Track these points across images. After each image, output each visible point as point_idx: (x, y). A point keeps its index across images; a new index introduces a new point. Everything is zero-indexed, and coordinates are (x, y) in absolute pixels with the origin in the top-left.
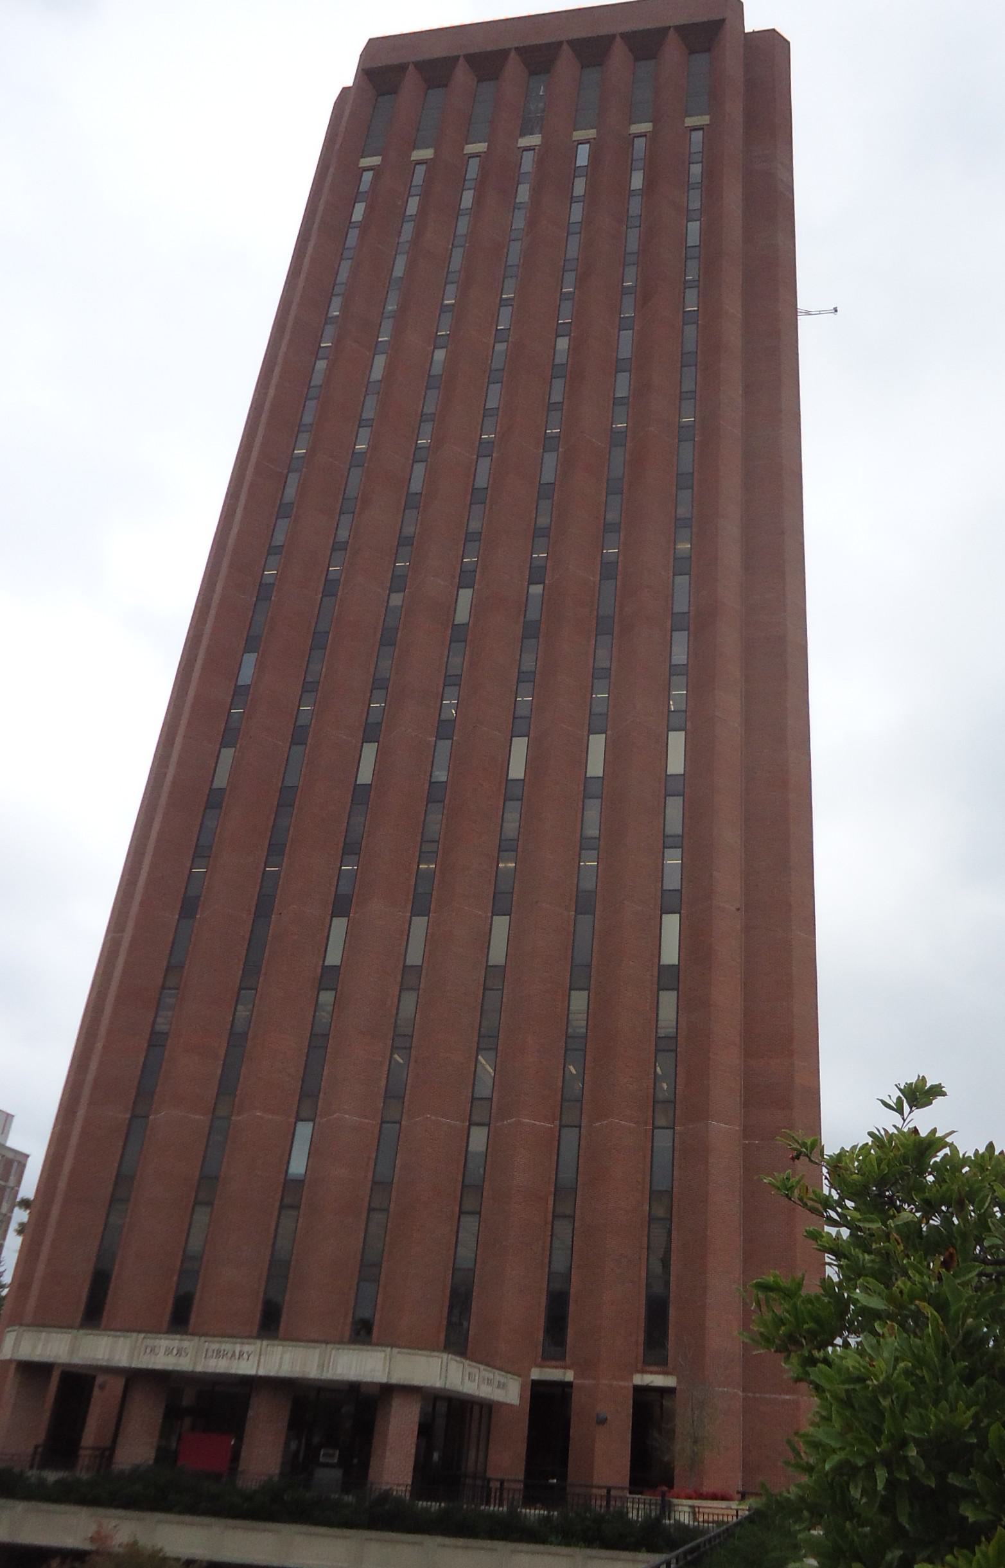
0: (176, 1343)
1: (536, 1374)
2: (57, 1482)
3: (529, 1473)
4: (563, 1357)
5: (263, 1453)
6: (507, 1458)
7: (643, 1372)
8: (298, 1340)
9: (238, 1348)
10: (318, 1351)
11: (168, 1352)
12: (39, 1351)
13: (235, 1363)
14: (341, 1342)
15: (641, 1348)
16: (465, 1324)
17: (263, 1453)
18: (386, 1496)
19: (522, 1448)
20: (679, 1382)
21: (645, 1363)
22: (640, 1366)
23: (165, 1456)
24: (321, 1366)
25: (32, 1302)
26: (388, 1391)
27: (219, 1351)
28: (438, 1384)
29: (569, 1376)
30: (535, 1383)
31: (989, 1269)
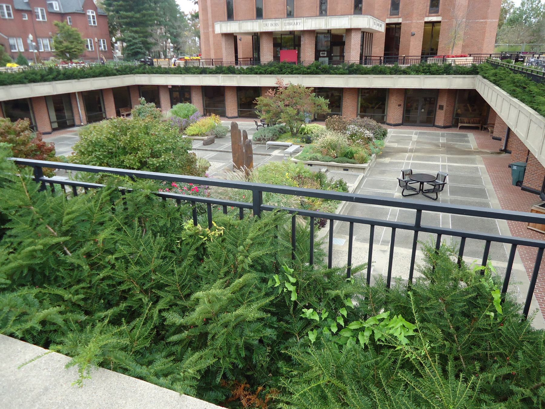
0: (274, 22)
1: (388, 21)
2: (247, 68)
3: (385, 54)
4: (437, 12)
5: (308, 54)
6: (378, 49)
7: (428, 16)
8: (335, 15)
9: (295, 21)
10: (324, 20)
11: (272, 25)
12: (229, 30)
13: (295, 26)
14: (316, 16)
15: (428, 8)
16: (360, 5)
17: (308, 54)
18: (352, 65)
19: (383, 46)
20: (442, 19)
21: (430, 13)
22: (427, 14)
23: (276, 57)
24: (326, 24)
25: (210, 15)
26: (349, 31)
27: (289, 23)
28: (367, 27)
29: (400, 20)
30: (387, 24)
31: (150, 23)
